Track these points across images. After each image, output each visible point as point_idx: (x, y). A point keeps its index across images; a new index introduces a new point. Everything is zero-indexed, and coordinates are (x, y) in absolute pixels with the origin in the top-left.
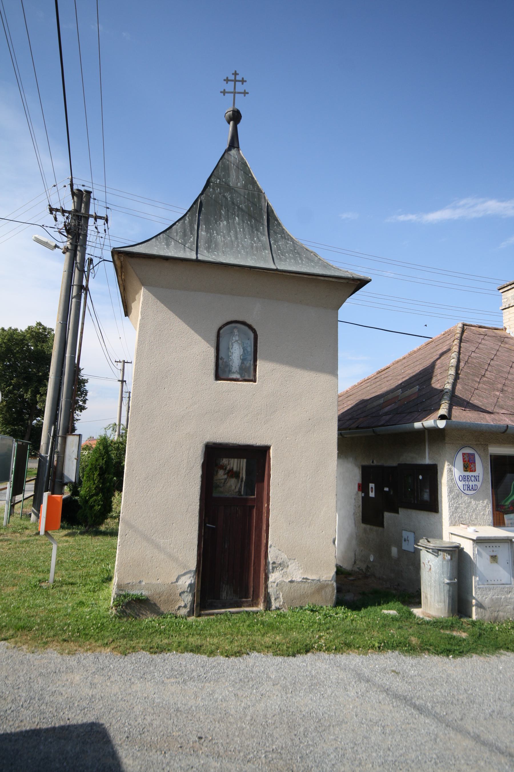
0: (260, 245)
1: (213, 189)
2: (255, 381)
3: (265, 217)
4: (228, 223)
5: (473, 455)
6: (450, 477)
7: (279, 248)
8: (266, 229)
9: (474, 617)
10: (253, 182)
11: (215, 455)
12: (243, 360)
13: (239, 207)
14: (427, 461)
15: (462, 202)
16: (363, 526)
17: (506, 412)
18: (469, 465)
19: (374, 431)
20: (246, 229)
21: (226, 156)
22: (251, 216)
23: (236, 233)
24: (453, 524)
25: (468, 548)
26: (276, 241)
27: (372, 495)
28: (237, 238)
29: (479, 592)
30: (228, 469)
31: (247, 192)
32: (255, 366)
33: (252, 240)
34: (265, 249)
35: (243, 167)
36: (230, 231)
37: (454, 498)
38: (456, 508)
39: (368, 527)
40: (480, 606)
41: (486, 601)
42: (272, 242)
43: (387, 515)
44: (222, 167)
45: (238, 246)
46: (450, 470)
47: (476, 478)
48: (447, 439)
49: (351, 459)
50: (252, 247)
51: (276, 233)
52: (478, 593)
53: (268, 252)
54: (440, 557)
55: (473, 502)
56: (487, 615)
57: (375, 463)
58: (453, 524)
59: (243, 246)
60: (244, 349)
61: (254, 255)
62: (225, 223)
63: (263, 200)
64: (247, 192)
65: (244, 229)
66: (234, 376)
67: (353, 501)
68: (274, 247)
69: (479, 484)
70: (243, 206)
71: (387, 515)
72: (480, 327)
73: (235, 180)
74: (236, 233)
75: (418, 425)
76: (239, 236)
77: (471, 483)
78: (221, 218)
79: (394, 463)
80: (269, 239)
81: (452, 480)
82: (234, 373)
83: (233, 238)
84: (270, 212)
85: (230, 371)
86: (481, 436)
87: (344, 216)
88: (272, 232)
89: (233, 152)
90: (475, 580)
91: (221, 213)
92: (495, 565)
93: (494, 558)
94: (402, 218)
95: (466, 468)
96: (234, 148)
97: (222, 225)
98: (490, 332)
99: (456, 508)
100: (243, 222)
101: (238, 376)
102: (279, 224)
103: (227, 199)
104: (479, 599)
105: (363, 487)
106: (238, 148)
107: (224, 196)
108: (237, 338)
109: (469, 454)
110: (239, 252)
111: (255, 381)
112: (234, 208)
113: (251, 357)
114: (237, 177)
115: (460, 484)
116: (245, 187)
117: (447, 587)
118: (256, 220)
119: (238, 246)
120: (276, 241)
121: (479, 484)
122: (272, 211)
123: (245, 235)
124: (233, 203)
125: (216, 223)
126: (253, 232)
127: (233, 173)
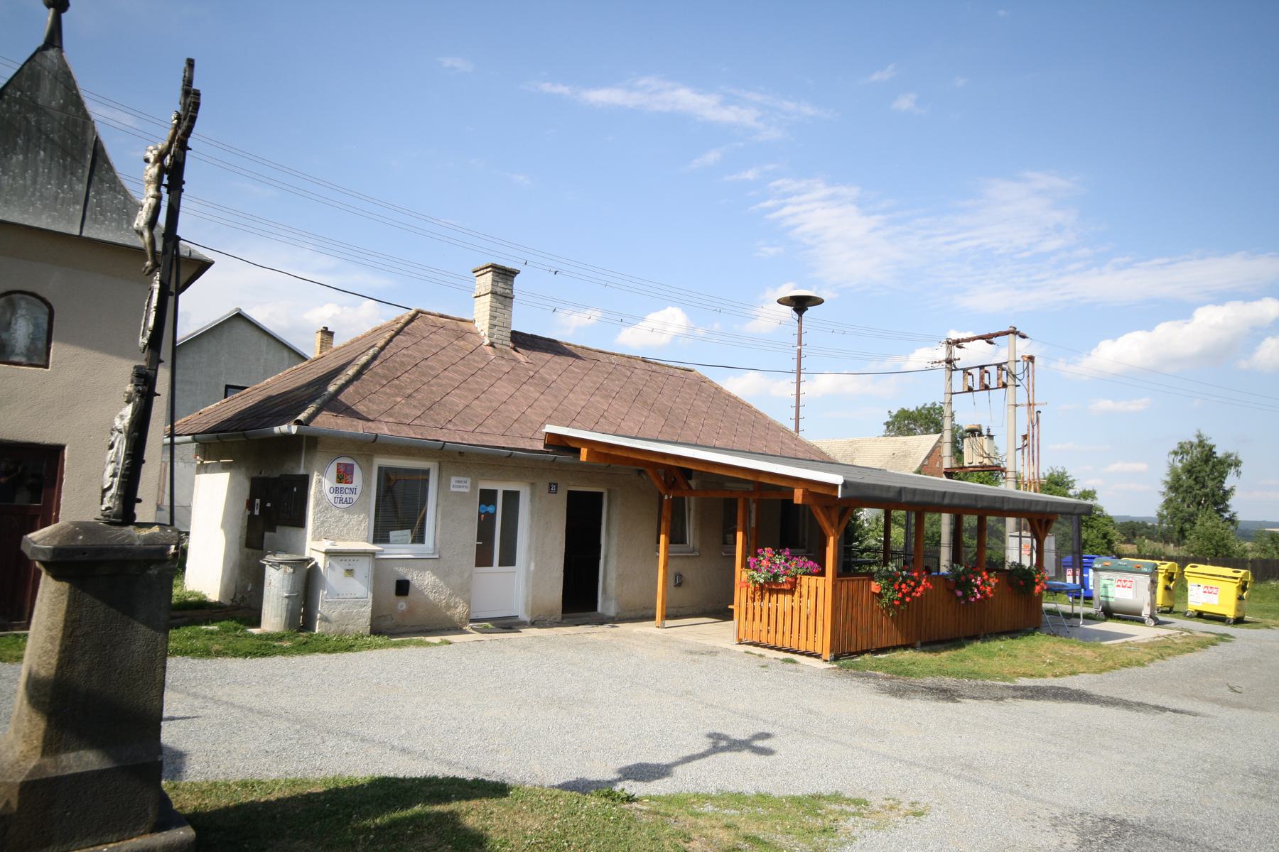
0: (70, 196)
1: (9, 104)
2: (47, 367)
3: (89, 156)
4: (26, 158)
5: (352, 466)
6: (322, 486)
7: (99, 204)
8: (87, 173)
9: (317, 631)
10: (78, 103)
11: (1094, 492)
12: (33, 340)
13: (48, 137)
14: (302, 471)
15: (642, 82)
16: (246, 550)
17: (391, 420)
18: (344, 475)
19: (244, 435)
20: (55, 171)
21: (37, 58)
22: (65, 152)
23: (36, 175)
24: (313, 539)
25: (320, 560)
26: (98, 193)
27: (257, 512)
28: (34, 182)
29: (326, 606)
30: (866, 543)
31: (65, 116)
32: (49, 349)
33: (60, 186)
34: (77, 203)
35: (66, 80)
36: (26, 171)
37: (323, 509)
38: (323, 523)
39: (250, 551)
40: (325, 619)
41: (333, 615)
42: (92, 193)
43: (267, 534)
44: (28, 73)
45: (33, 194)
46: (320, 481)
47: (353, 491)
48: (319, 447)
49: (243, 470)
50: (56, 198)
51: (102, 181)
52: (325, 605)
53: (79, 207)
54: (282, 570)
55: (346, 516)
56: (333, 628)
57: (263, 475)
58: (313, 539)
59: (41, 195)
60: (36, 326)
61: (55, 210)
62: (21, 157)
63: (90, 132)
64: (65, 116)
65: (50, 170)
66: (16, 359)
67: (240, 521)
68: (93, 201)
69: (355, 497)
70: (55, 137)
71: (267, 534)
72: (442, 316)
73: (47, 95)
74: (36, 175)
75: (276, 429)
76: (40, 179)
77: (344, 496)
78: (15, 149)
79: (276, 474)
80: (88, 188)
81: (321, 492)
82: (17, 355)
83: (29, 182)
84: (98, 151)
85: (13, 352)
86: (369, 447)
87: (448, 62)
88: (96, 178)
89: (51, 53)
90: (322, 594)
91: (16, 143)
92: (350, 580)
93: (350, 572)
94: (547, 87)
95: (340, 479)
96: (54, 46)
97: (14, 160)
98: (451, 324)
99: (323, 523)
100: (52, 159)
101: (23, 360)
102: (111, 168)
103: (29, 122)
104: (325, 613)
105: (250, 505)
106: (60, 47)
107: (26, 118)
108: (23, 312)
109: (346, 465)
110: (33, 204)
111: (47, 367)
112: (39, 138)
113: (44, 337)
114: (53, 93)
115: (331, 497)
116: (63, 108)
117: (286, 601)
118: (73, 158)
119: (33, 194)
120: (98, 193)
121: (355, 497)
122: (103, 150)
123: (50, 179)
124: (39, 130)
125: (5, 156)
126: (64, 176)
127: (46, 86)
